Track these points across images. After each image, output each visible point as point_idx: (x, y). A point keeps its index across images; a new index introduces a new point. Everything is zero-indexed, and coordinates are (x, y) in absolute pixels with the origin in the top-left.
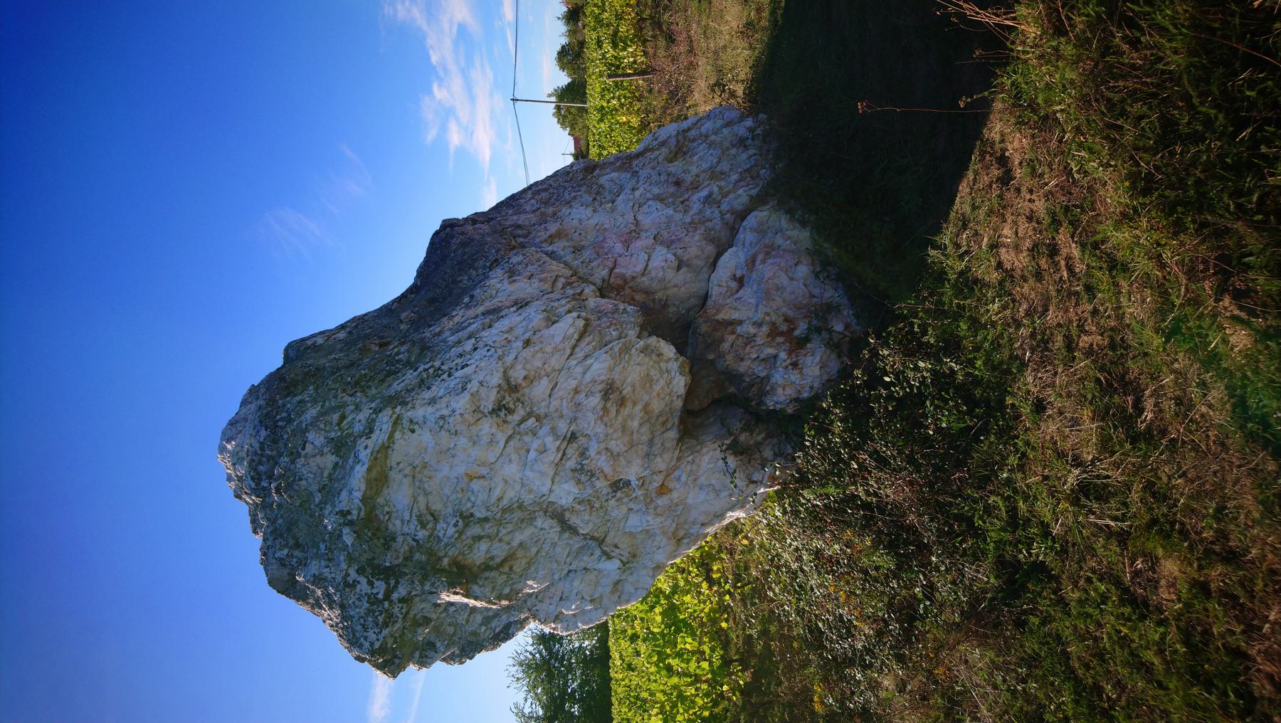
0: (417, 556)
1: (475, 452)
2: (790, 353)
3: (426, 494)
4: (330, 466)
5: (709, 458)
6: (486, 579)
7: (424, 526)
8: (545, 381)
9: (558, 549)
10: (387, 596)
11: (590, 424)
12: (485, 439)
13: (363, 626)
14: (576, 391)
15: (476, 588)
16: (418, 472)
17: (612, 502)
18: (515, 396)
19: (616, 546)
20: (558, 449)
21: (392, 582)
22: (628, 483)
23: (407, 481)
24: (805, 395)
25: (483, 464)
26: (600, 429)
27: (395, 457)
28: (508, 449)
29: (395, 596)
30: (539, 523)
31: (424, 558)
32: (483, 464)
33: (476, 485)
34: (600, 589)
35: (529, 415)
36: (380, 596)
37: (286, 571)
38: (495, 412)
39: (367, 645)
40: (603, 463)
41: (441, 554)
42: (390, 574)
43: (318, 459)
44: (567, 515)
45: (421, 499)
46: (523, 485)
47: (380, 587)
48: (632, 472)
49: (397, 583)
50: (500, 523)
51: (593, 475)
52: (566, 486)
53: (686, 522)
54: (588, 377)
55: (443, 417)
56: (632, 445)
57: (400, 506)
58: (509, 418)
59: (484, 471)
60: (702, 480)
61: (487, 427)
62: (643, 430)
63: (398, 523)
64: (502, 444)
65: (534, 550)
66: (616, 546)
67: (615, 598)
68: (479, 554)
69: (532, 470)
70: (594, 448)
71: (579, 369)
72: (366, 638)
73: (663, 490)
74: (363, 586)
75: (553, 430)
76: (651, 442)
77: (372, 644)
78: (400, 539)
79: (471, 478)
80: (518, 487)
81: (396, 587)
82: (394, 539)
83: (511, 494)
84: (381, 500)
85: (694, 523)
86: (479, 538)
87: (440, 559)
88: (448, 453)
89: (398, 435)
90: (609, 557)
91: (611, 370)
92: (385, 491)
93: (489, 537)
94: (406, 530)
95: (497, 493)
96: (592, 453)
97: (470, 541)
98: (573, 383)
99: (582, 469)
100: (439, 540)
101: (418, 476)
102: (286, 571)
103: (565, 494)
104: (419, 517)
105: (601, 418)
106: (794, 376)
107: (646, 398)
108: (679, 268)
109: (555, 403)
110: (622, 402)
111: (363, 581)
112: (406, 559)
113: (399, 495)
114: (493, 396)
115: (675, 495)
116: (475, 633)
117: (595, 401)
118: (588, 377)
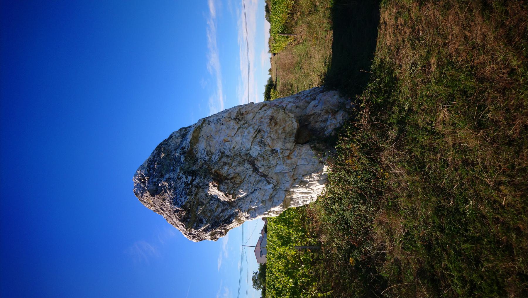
0: (204, 166)
1: (228, 131)
2: (332, 116)
3: (210, 146)
4: (180, 142)
5: (306, 150)
6: (226, 183)
7: (208, 155)
8: (252, 114)
9: (251, 178)
10: (191, 183)
11: (265, 127)
12: (231, 127)
13: (181, 195)
14: (261, 118)
15: (222, 186)
16: (209, 138)
17: (271, 157)
18: (242, 117)
19: (272, 178)
20: (254, 133)
21: (194, 177)
22: (277, 151)
23: (205, 141)
24: (338, 126)
25: (229, 136)
26: (268, 129)
27: (202, 133)
28: (238, 132)
29: (194, 183)
30: (246, 166)
31: (206, 167)
32: (229, 136)
33: (226, 144)
34: (265, 197)
35: (246, 123)
36: (189, 182)
37: (155, 187)
38: (235, 119)
39: (180, 203)
40: (268, 141)
41: (212, 167)
42: (193, 173)
43: (176, 140)
44: (256, 162)
45: (208, 147)
46: (242, 145)
47: (190, 178)
48: (278, 146)
49: (196, 178)
50: (233, 160)
51: (265, 145)
52: (256, 147)
53: (297, 174)
54: (265, 115)
55: (219, 119)
56: (278, 138)
57: (201, 149)
58: (240, 122)
59: (229, 139)
60: (303, 156)
61: (232, 123)
62: (283, 134)
63: (200, 154)
64: (237, 129)
65: (243, 177)
66: (272, 178)
67: (270, 204)
68: (225, 171)
69: (245, 139)
70: (266, 135)
71: (263, 113)
72: (180, 200)
73: (289, 157)
74: (184, 179)
75: (253, 128)
76: (285, 139)
77: (182, 203)
78: (199, 160)
79: (225, 141)
80: (240, 145)
81: (195, 180)
82: (197, 160)
83: (237, 147)
84: (195, 147)
85: (300, 174)
86: (225, 163)
87: (212, 169)
88: (218, 131)
89: (204, 125)
90: (269, 183)
91: (273, 113)
92: (197, 145)
93: (229, 164)
94: (202, 157)
95: (233, 146)
96: (265, 137)
97: (222, 164)
98: (261, 116)
99: (262, 142)
100: (213, 161)
101: (208, 140)
102: (155, 187)
103: (255, 151)
104: (207, 152)
105: (269, 126)
106: (334, 121)
107: (284, 125)
108: (296, 108)
109: (254, 121)
110: (276, 123)
111: (184, 176)
112: (200, 168)
113: (202, 146)
114: (235, 114)
115: (293, 160)
116: (217, 217)
117: (267, 120)
118: (265, 115)
